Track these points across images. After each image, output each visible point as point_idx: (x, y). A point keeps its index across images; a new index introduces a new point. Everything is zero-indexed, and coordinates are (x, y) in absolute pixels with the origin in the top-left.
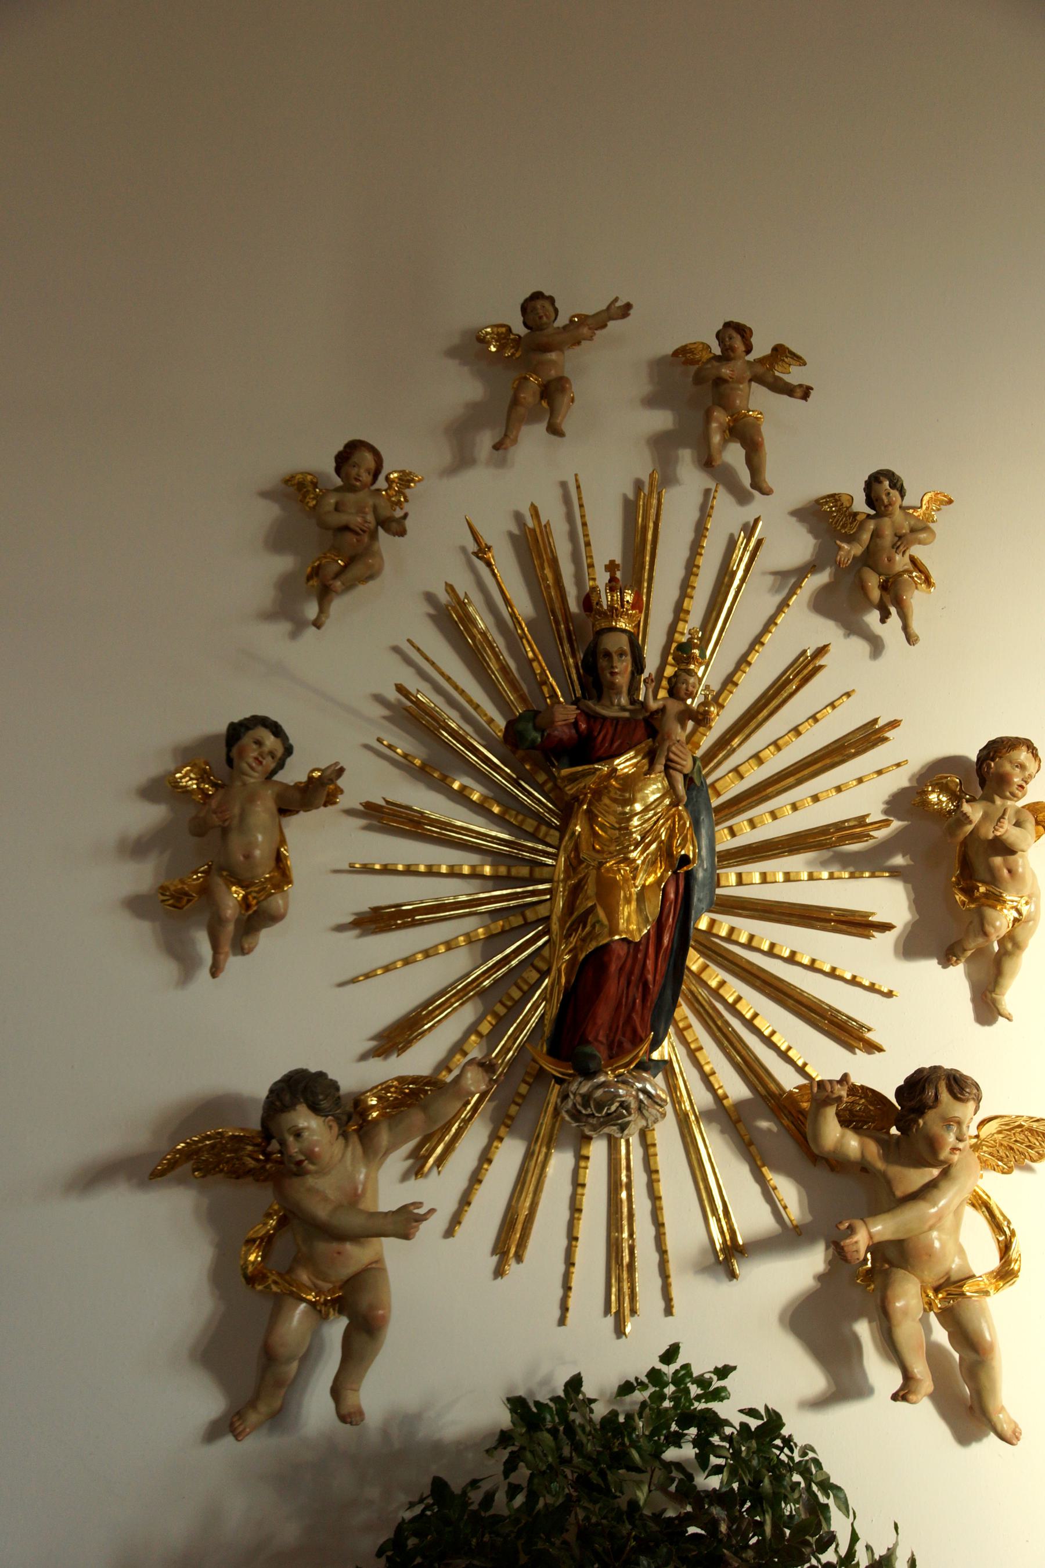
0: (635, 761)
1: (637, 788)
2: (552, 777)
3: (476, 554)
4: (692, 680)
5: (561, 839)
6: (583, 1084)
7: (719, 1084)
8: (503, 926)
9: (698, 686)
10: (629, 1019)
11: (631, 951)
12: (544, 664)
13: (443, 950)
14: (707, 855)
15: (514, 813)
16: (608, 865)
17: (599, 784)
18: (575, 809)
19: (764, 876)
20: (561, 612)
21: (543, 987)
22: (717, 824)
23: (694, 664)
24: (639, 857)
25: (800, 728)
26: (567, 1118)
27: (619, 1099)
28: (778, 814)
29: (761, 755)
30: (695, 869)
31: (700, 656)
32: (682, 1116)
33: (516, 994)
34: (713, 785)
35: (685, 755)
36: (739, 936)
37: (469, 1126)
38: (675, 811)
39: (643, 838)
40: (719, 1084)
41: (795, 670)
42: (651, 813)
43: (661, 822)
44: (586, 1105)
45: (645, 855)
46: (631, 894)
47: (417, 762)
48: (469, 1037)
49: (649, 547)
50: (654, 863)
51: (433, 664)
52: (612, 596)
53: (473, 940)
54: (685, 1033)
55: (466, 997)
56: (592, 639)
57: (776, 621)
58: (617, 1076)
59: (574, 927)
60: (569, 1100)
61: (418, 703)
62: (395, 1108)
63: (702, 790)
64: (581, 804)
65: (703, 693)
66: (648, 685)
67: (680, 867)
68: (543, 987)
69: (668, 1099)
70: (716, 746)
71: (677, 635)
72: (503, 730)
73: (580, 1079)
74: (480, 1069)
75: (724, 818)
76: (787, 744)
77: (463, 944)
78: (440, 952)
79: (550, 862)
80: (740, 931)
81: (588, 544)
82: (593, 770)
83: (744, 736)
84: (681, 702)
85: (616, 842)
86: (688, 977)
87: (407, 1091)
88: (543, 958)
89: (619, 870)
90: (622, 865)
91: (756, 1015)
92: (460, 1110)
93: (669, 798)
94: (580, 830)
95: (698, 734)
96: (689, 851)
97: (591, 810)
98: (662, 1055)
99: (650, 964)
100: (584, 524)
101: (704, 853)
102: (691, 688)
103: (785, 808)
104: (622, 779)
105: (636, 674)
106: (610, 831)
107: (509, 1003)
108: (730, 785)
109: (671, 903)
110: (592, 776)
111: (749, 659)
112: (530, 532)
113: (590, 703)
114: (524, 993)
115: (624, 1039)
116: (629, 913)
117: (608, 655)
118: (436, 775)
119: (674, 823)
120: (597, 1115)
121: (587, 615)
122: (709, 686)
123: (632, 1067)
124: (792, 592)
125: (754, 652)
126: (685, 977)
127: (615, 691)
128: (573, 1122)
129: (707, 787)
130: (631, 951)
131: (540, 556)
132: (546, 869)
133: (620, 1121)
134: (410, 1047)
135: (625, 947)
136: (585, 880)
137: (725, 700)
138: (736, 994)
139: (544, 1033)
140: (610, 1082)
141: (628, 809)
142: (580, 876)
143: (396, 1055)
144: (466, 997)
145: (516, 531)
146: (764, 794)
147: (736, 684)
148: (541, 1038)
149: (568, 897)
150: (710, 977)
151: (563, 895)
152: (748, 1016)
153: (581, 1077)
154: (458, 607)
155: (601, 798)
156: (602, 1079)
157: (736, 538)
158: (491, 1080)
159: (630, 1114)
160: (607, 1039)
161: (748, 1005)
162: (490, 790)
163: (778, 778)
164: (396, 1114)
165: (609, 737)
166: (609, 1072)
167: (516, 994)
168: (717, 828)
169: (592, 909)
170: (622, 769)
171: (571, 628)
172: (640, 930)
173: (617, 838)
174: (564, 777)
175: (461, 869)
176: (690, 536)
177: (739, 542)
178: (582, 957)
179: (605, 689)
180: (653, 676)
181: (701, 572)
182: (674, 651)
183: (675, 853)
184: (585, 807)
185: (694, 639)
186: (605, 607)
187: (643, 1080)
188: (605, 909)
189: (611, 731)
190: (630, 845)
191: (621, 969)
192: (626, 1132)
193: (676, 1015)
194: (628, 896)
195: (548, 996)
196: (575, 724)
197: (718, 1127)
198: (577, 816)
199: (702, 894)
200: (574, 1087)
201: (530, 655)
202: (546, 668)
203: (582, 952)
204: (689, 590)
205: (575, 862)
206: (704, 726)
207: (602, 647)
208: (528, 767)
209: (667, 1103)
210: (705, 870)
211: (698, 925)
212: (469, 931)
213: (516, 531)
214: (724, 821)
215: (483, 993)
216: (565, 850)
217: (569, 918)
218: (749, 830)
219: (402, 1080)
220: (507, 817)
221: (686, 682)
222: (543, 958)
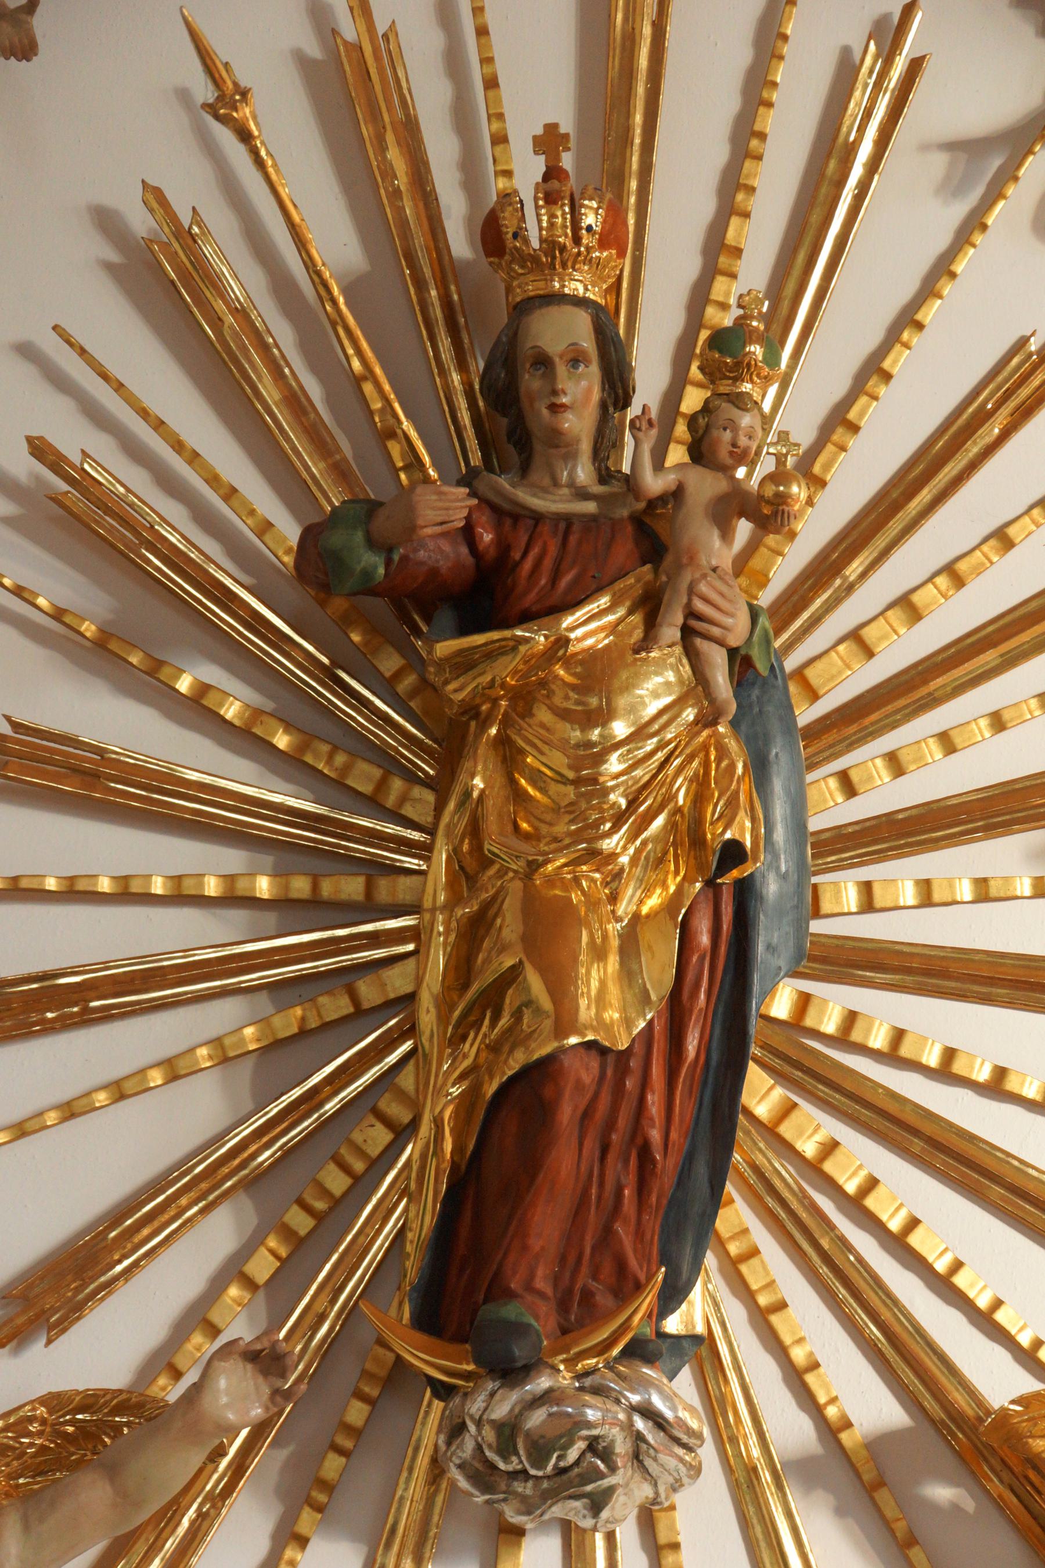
0: (611, 618)
1: (616, 684)
2: (415, 662)
3: (211, 108)
4: (746, 420)
5: (439, 809)
6: (497, 1397)
7: (793, 1333)
8: (303, 1019)
9: (760, 433)
10: (607, 1233)
11: (609, 1072)
12: (387, 387)
13: (159, 1082)
14: (786, 841)
15: (325, 748)
16: (550, 867)
17: (526, 676)
18: (471, 738)
19: (925, 886)
20: (430, 259)
21: (400, 1164)
22: (812, 767)
23: (752, 381)
24: (625, 848)
25: (1011, 531)
26: (463, 1483)
27: (585, 1433)
28: (958, 740)
29: (917, 598)
30: (757, 875)
31: (765, 360)
32: (741, 1475)
33: (337, 1182)
34: (799, 673)
35: (730, 601)
36: (868, 1031)
37: (224, 1511)
38: (710, 737)
39: (633, 802)
40: (793, 1333)
41: (999, 388)
42: (651, 744)
43: (677, 762)
44: (506, 1449)
45: (638, 842)
46: (605, 937)
47: (89, 629)
48: (224, 1289)
49: (640, 90)
50: (660, 861)
51: (119, 387)
52: (552, 216)
53: (231, 1054)
54: (744, 1268)
55: (216, 1193)
56: (506, 320)
57: (953, 268)
58: (579, 1377)
59: (472, 1018)
60: (467, 1436)
61: (83, 483)
62: (39, 1474)
63: (774, 686)
64: (484, 725)
65: (772, 450)
66: (640, 435)
67: (723, 868)
68: (400, 1164)
69: (706, 1432)
70: (808, 578)
71: (710, 311)
72: (295, 548)
73: (490, 1386)
74: (249, 1366)
75: (827, 754)
76: (979, 570)
77: (208, 1064)
78: (152, 1085)
79: (411, 863)
80: (870, 1020)
81: (491, 83)
82: (511, 643)
83: (875, 554)
84: (720, 475)
85: (570, 813)
86: (747, 1133)
87: (70, 1429)
88: (401, 1095)
89: (576, 880)
90: (584, 868)
91: (913, 1223)
92: (200, 1471)
93: (692, 706)
94: (482, 786)
95: (763, 550)
96: (742, 831)
97: (508, 737)
98: (690, 1322)
99: (654, 1102)
100: (482, 32)
101: (780, 835)
102: (743, 441)
103: (974, 726)
104: (582, 663)
105: (611, 409)
106: (554, 788)
107: (320, 1205)
108: (840, 673)
109: (702, 958)
110: (510, 657)
111: (886, 365)
112: (347, 51)
113: (503, 482)
114: (357, 1179)
115: (593, 1285)
116: (603, 983)
117: (543, 362)
118: (134, 660)
119: (706, 764)
120: (533, 1472)
121: (491, 264)
122: (787, 433)
123: (616, 1352)
124: (994, 194)
125: (898, 347)
126: (740, 1134)
127: (563, 450)
128: (477, 1493)
129: (785, 678)
130: (609, 1072)
131: (374, 115)
132: (404, 881)
133: (589, 1488)
134: (79, 1318)
135: (595, 1064)
136: (496, 906)
137: (827, 467)
138: (863, 1174)
139: (405, 1276)
140: (562, 1390)
141: (595, 734)
142: (485, 896)
143: (43, 1340)
144: (216, 1193)
145: (314, 50)
146: (923, 691)
147: (854, 428)
148: (399, 1288)
149: (456, 945)
150: (800, 1133)
151: (445, 944)
152: (895, 1225)
153: (494, 1381)
154: (176, 245)
155: (531, 709)
156: (543, 1382)
157: (857, 61)
158: (276, 1392)
159: (613, 1469)
160: (555, 1286)
161: (895, 1199)
162: (270, 697)
163: (958, 652)
164: (41, 1490)
165: (548, 563)
166: (562, 1367)
167: (337, 1182)
168: (810, 777)
169: (514, 974)
170: (579, 640)
171: (456, 297)
172: (628, 1022)
173: (571, 804)
174: (441, 659)
175: (201, 885)
176: (742, 56)
177: (864, 70)
178: (491, 1089)
179: (538, 447)
180: (654, 414)
181: (771, 150)
182: (702, 350)
183: (709, 836)
184: (493, 731)
185: (752, 318)
186: (535, 244)
187: (646, 1384)
188: (544, 972)
189: (553, 550)
190: (602, 821)
191: (587, 1114)
192: (605, 1514)
193: (718, 1224)
194: (599, 941)
195: (413, 1186)
196: (468, 532)
197: (831, 1499)
198: (475, 752)
199: (776, 935)
200: (476, 1406)
201: (356, 364)
202: (392, 396)
203: (491, 1078)
204: (740, 197)
205: (471, 864)
206: (777, 532)
207: (529, 344)
208: (356, 638)
209: (703, 1441)
210: (784, 877)
211: (768, 1006)
212: (221, 1032)
213: (314, 50)
214: (828, 759)
215: (255, 1182)
216: (448, 835)
217: (461, 997)
218: (887, 779)
219: (55, 1401)
220: (309, 759)
221: (732, 425)
222: (401, 1095)
